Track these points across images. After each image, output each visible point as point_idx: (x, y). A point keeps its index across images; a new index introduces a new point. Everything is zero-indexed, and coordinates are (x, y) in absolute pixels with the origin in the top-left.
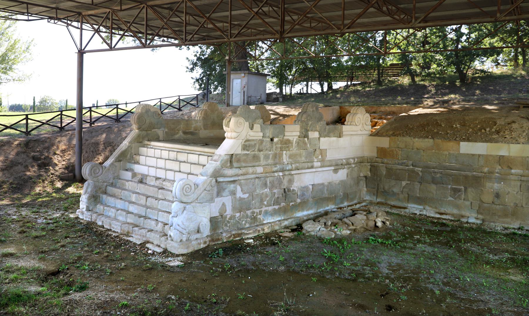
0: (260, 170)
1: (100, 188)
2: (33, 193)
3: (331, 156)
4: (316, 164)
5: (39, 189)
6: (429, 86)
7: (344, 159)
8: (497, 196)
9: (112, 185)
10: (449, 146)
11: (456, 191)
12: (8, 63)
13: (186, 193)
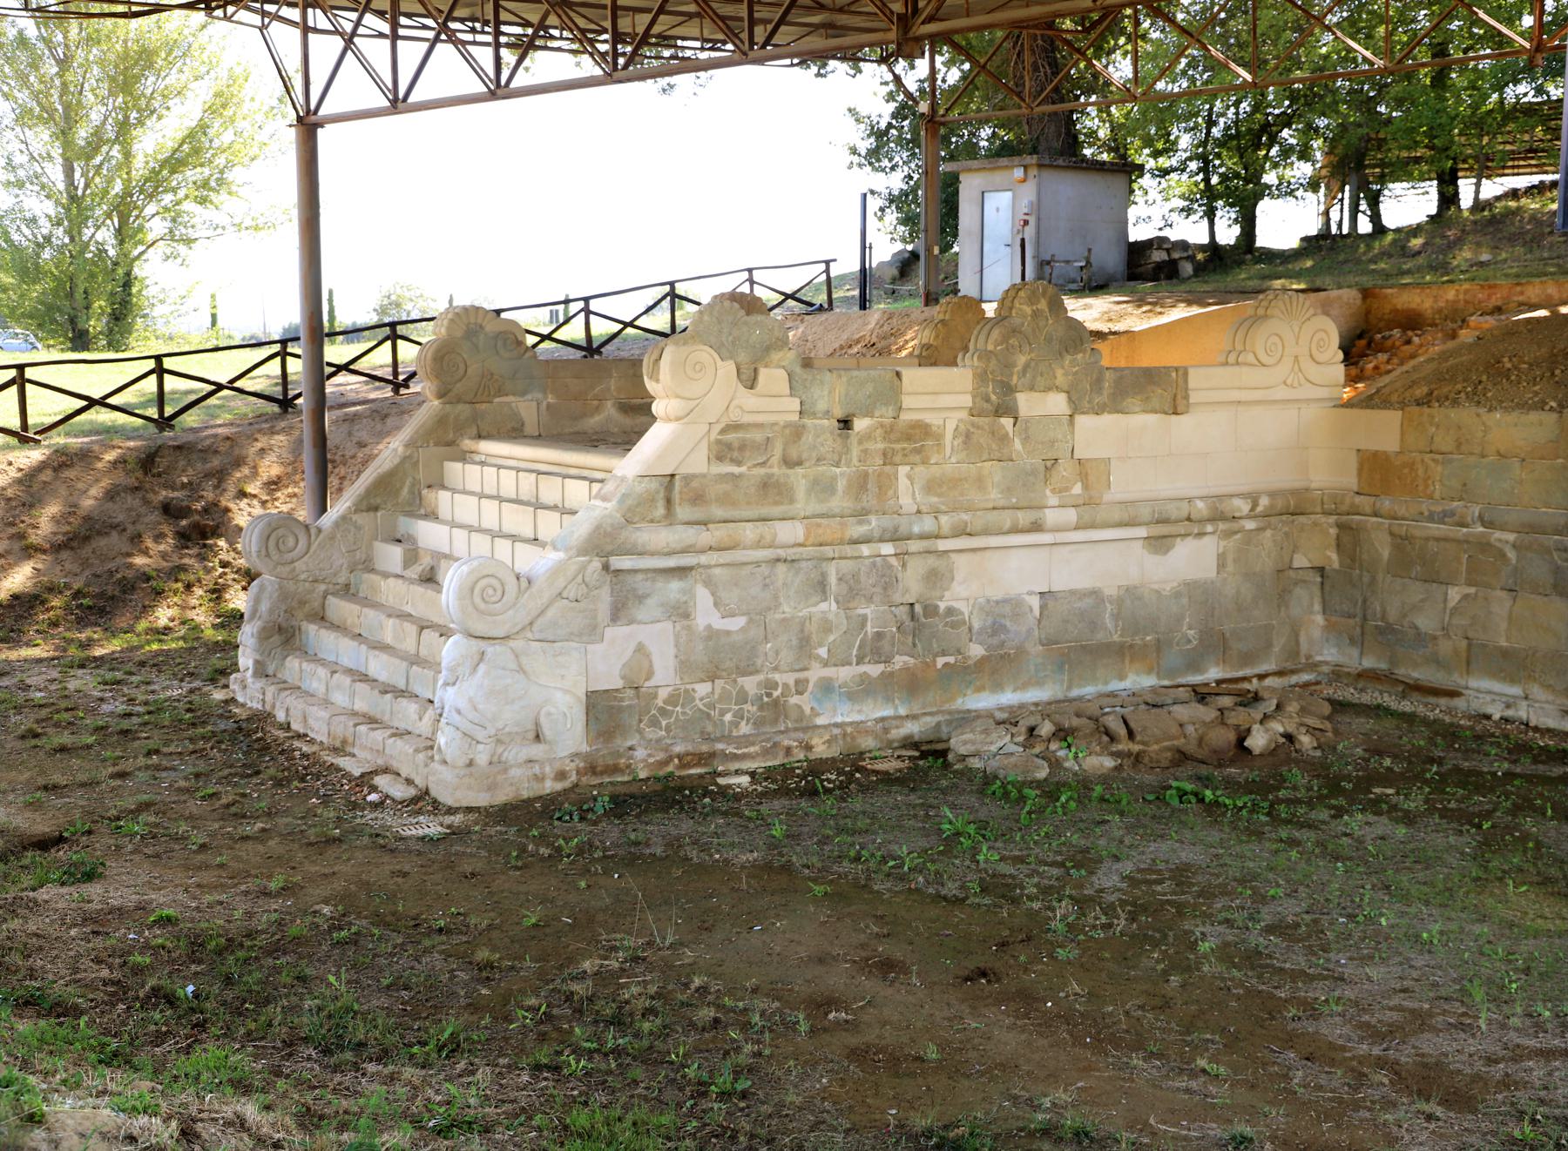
0: (791, 532)
1: (302, 603)
2: (142, 625)
3: (1124, 485)
4: (1051, 516)
5: (170, 612)
9: (347, 591)
13: (482, 606)
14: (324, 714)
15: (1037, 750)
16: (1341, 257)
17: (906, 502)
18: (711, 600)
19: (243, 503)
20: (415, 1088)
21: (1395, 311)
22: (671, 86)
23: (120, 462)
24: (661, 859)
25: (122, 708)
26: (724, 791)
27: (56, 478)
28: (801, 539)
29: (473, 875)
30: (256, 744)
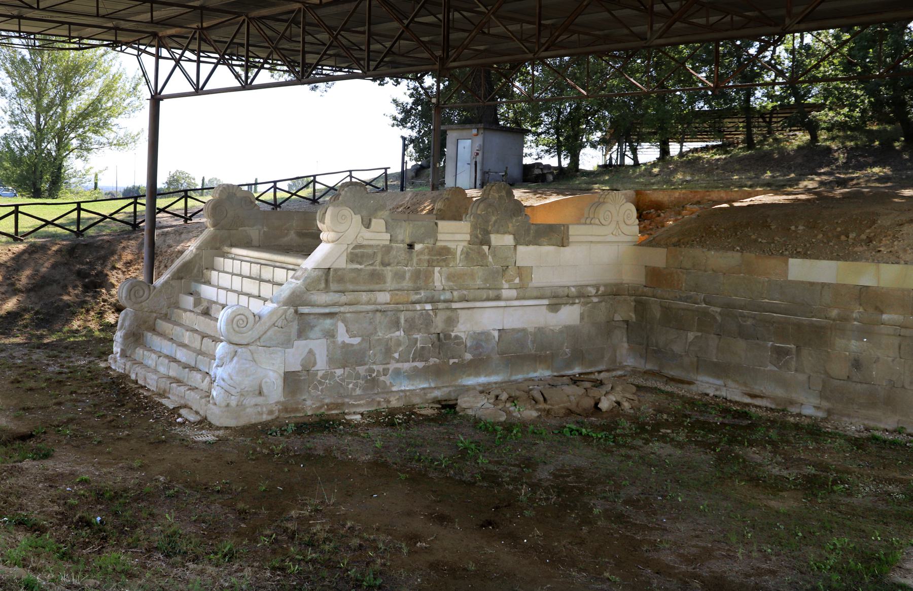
0: (383, 297)
1: (145, 322)
2: (66, 329)
3: (539, 279)
4: (505, 293)
5: (79, 323)
6: (837, 150)
9: (166, 318)
10: (768, 268)
11: (780, 353)
12: (101, 114)
13: (237, 329)
14: (155, 377)
15: (500, 407)
16: (622, 175)
17: (438, 284)
19: (114, 272)
20: (213, 578)
21: (651, 201)
22: (317, 87)
24: (323, 457)
25: (58, 369)
26: (349, 423)
27: (30, 258)
28: (388, 301)
29: (232, 462)
30: (122, 391)
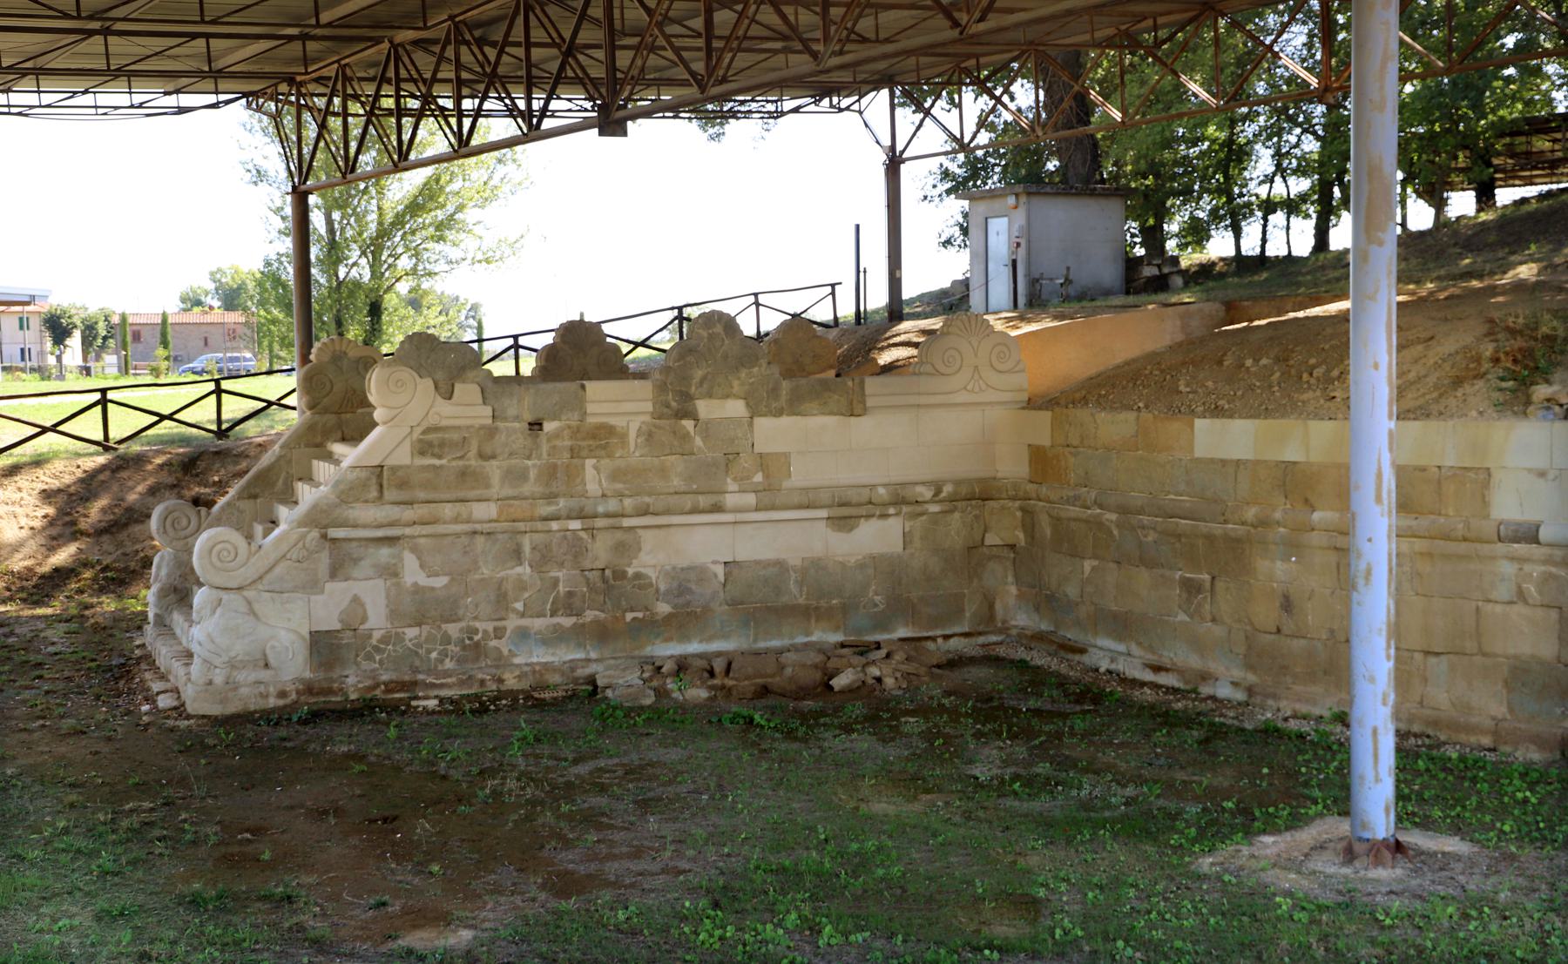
0: (484, 511)
3: (801, 475)
4: (730, 500)
7: (884, 485)
8: (1287, 605)
13: (218, 564)
17: (593, 488)
18: (417, 563)
23: (168, 464)
